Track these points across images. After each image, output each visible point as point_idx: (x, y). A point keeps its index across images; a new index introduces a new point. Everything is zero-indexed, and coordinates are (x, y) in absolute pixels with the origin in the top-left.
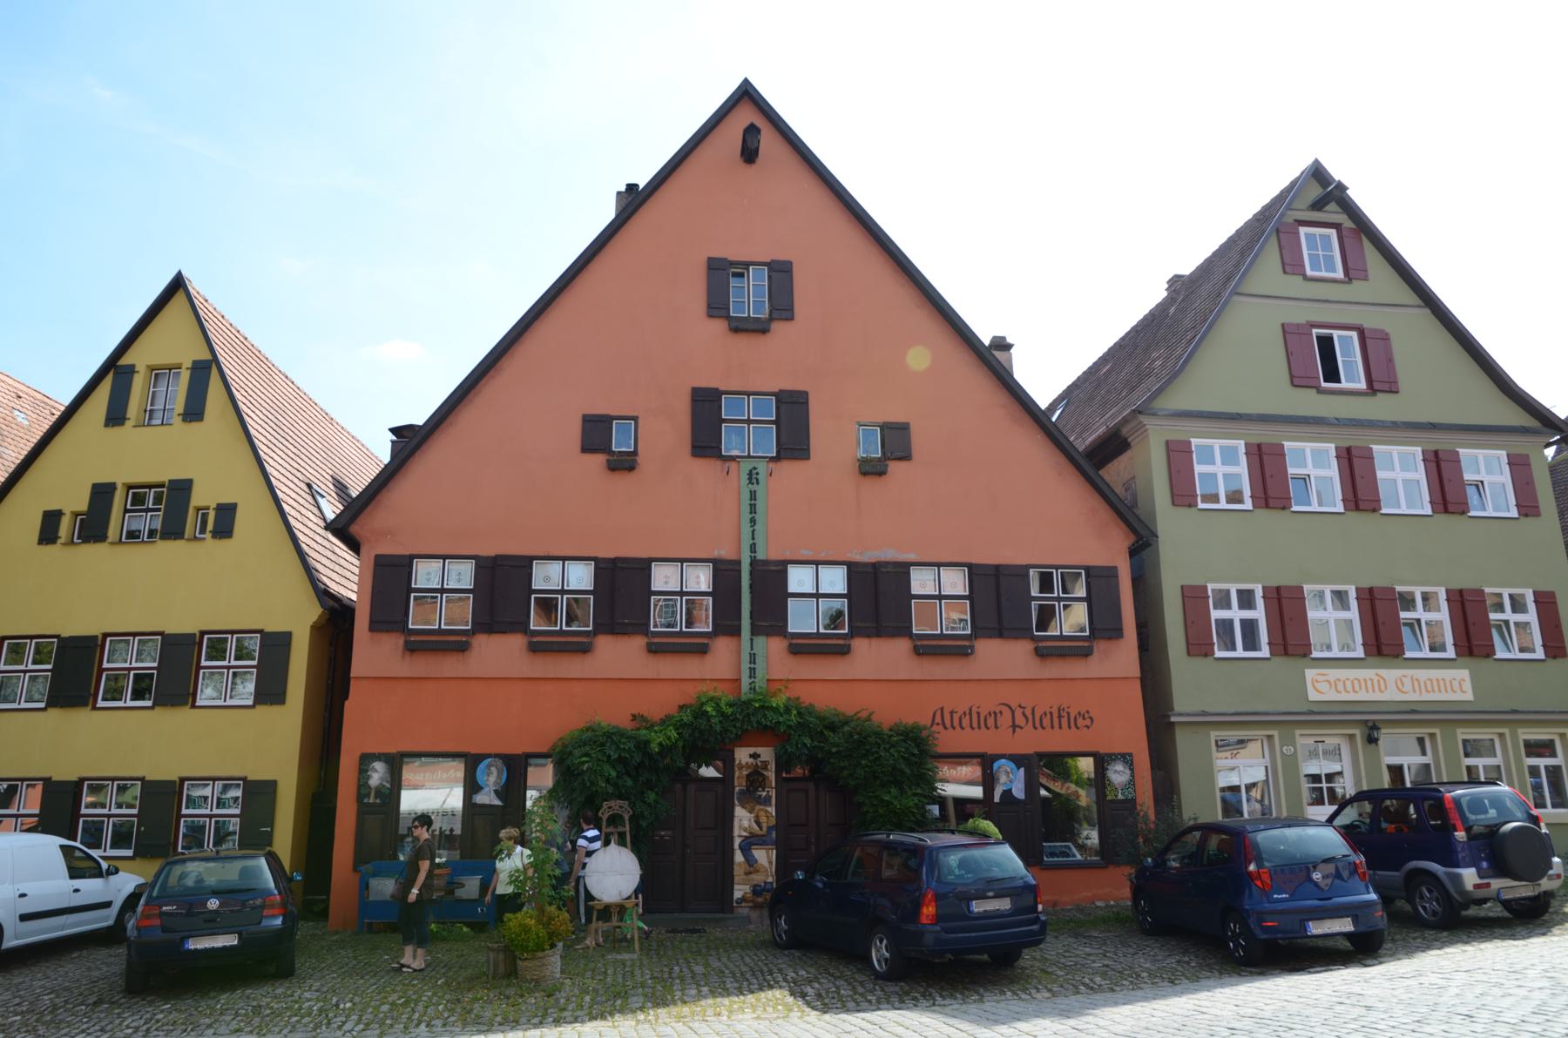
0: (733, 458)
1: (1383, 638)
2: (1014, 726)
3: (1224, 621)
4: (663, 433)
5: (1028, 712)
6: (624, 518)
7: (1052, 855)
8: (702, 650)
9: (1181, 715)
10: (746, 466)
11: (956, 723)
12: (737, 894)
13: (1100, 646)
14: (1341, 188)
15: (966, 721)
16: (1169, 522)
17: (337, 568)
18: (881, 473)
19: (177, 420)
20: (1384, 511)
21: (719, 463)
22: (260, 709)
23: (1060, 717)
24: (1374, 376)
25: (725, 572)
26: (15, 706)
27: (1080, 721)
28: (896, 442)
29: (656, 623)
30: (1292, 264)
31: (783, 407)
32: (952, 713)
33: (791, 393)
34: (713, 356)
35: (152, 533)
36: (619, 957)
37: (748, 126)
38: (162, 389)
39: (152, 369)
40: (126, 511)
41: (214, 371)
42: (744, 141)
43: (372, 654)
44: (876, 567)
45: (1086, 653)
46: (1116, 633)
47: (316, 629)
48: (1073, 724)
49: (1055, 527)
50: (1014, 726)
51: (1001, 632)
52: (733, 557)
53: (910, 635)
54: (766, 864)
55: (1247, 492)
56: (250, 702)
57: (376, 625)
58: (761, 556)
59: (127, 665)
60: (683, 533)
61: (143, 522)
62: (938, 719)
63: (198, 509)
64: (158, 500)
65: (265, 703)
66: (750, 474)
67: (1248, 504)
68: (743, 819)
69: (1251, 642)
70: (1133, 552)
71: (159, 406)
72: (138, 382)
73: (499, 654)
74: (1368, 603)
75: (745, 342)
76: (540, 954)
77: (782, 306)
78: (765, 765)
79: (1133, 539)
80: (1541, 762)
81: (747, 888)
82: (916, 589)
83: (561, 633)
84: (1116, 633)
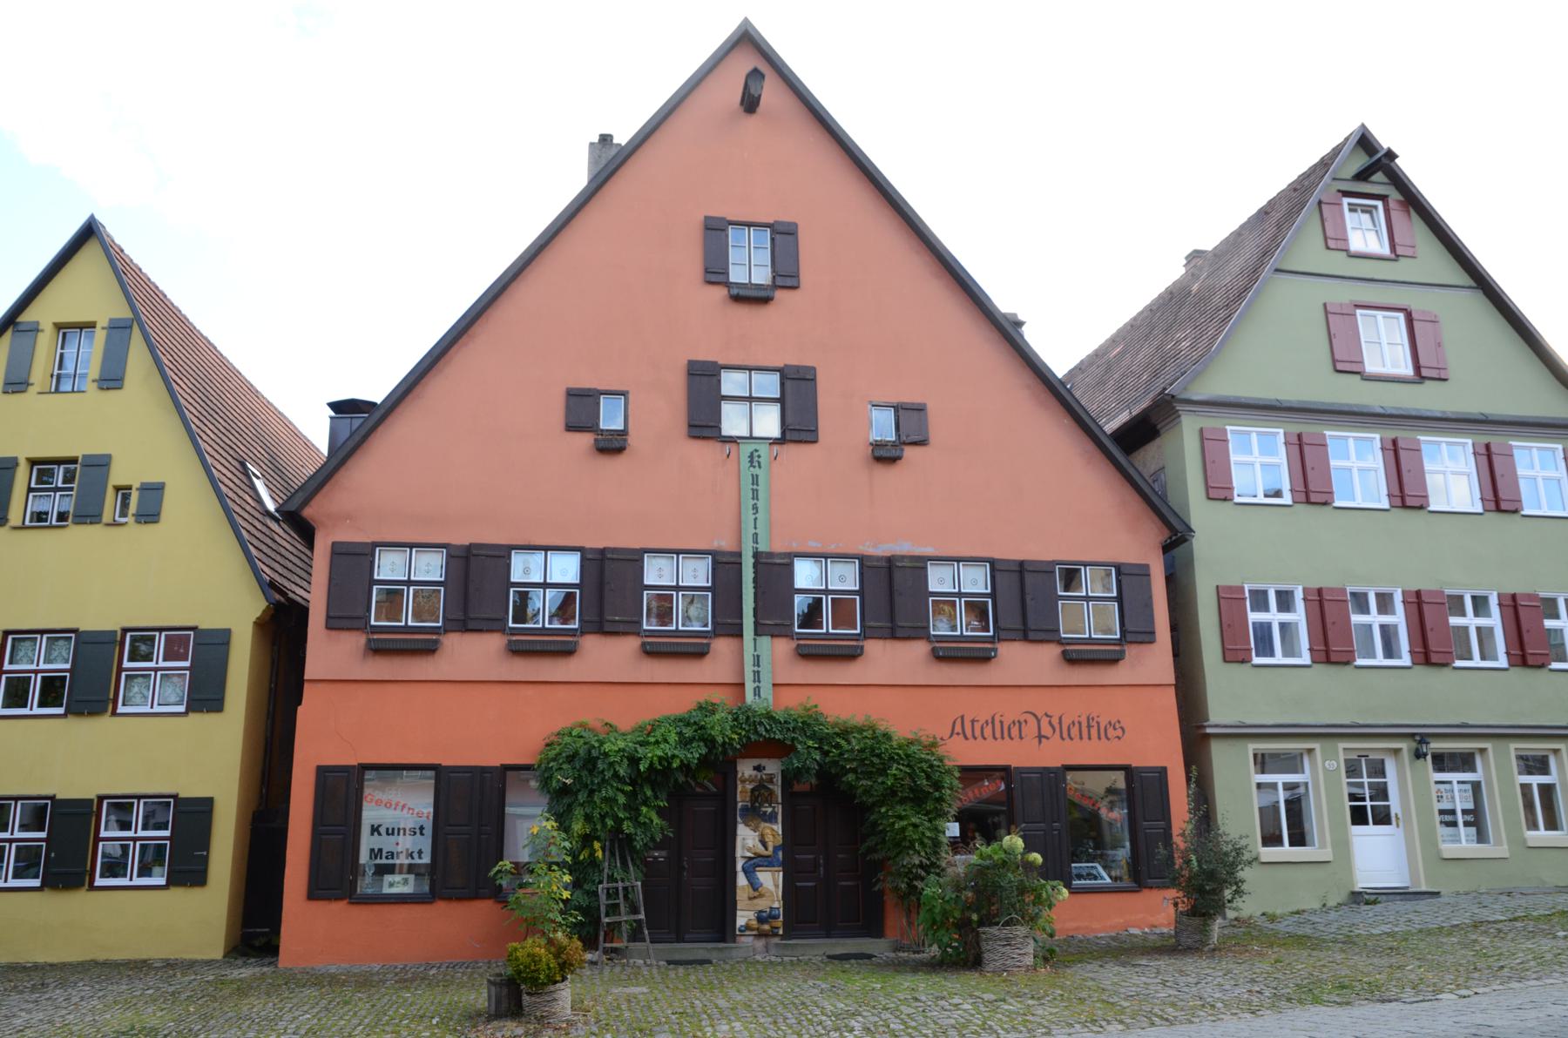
0: (732, 440)
1: (1332, 647)
2: (1040, 737)
3: (1261, 624)
4: (653, 413)
5: (1055, 721)
6: (616, 504)
7: (1079, 877)
8: (700, 654)
9: (1216, 726)
10: (746, 449)
11: (978, 733)
12: (741, 921)
13: (1131, 651)
14: (1391, 155)
15: (988, 731)
16: (1200, 514)
17: (278, 558)
18: (893, 460)
19: (91, 387)
20: (1337, 504)
21: (718, 445)
22: (195, 718)
23: (1089, 727)
24: (1422, 362)
25: (725, 566)
26: (147, 709)
27: (1110, 730)
28: (912, 425)
29: (940, 629)
30: (1335, 242)
31: (788, 383)
32: (973, 721)
33: (798, 368)
34: (707, 326)
35: (62, 517)
36: (628, 990)
37: (752, 72)
38: (70, 351)
39: (59, 327)
40: (30, 490)
41: (136, 328)
42: (746, 86)
43: (328, 653)
44: (890, 563)
45: (1113, 660)
46: (1147, 636)
47: (260, 625)
48: (1103, 735)
49: (1075, 516)
50: (1040, 737)
51: (893, 634)
52: (734, 549)
53: (928, 638)
54: (772, 888)
55: (1286, 487)
56: (182, 709)
57: (335, 623)
58: (762, 547)
59: (33, 667)
60: (678, 522)
61: (54, 504)
62: (958, 729)
63: (117, 489)
64: (69, 478)
65: (195, 711)
66: (751, 456)
67: (1287, 499)
68: (747, 839)
69: (1289, 650)
70: (1167, 548)
71: (69, 368)
72: (45, 342)
73: (474, 654)
74: (1414, 608)
75: (743, 311)
76: (552, 988)
77: (786, 276)
78: (771, 779)
79: (1167, 533)
80: (1535, 780)
81: (751, 915)
82: (649, 580)
83: (407, 629)
84: (1148, 637)
